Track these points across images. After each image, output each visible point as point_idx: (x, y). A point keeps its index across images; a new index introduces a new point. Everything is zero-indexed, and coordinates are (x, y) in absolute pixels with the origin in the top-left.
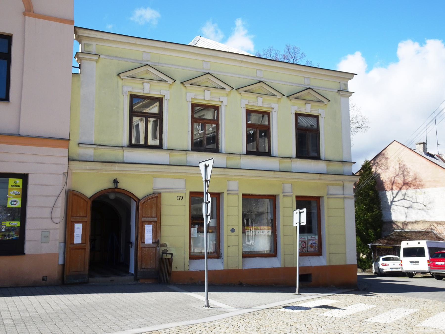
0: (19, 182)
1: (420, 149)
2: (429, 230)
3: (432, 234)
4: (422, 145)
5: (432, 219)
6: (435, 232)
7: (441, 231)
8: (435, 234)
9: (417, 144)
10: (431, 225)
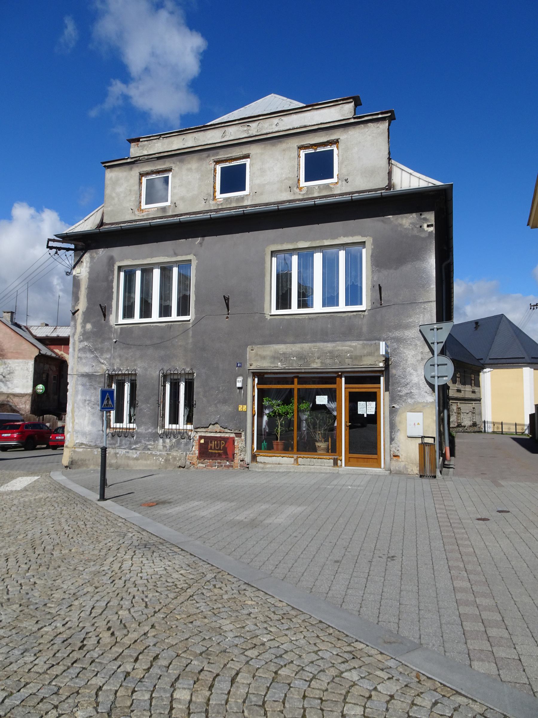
0: (50, 242)
1: (8, 316)
2: (5, 403)
3: (8, 406)
4: (10, 314)
5: (10, 391)
6: (11, 404)
7: (17, 403)
8: (10, 406)
9: (5, 312)
10: (8, 397)
